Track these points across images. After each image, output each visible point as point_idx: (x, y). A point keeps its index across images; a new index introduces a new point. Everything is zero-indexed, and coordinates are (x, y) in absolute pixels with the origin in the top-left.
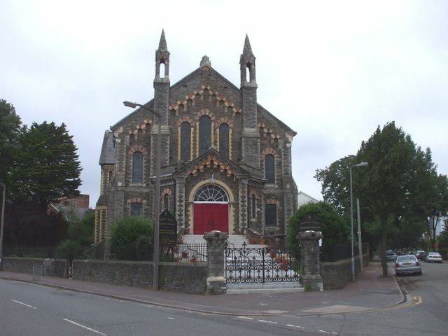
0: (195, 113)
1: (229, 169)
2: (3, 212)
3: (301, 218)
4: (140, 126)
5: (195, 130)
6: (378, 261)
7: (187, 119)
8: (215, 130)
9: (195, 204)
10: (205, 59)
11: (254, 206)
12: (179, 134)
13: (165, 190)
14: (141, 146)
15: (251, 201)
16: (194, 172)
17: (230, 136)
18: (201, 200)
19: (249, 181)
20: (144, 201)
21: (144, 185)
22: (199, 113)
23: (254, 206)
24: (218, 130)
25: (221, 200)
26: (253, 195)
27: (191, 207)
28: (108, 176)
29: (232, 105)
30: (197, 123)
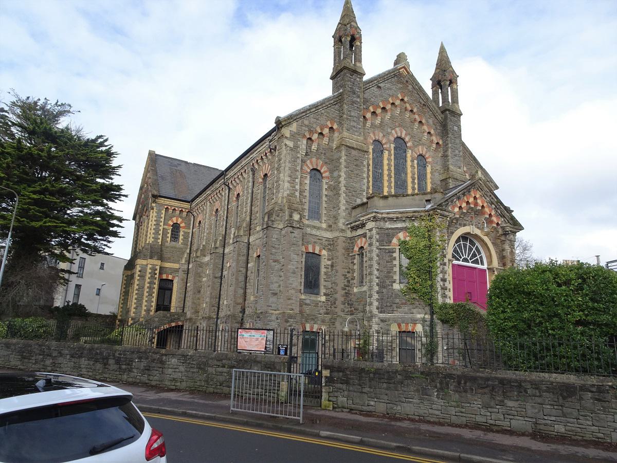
0: (389, 130)
2: (344, 435)
3: (136, 256)
4: (322, 129)
5: (390, 155)
7: (379, 136)
8: (412, 161)
10: (401, 58)
13: (359, 241)
14: (314, 160)
17: (429, 176)
20: (324, 252)
21: (324, 226)
24: (416, 162)
28: (163, 216)
30: (393, 146)
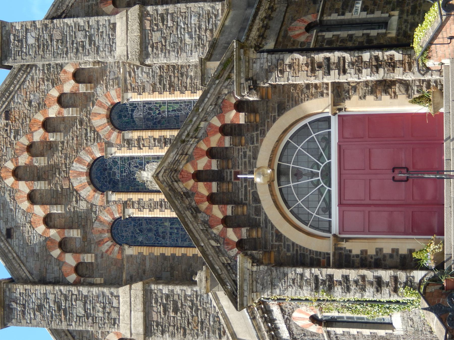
1: (194, 165)
6: (45, 187)
8: (129, 143)
9: (342, 229)
11: (341, 25)
12: (145, 250)
15: (328, 35)
16: (232, 235)
18: (327, 209)
19: (259, 49)
22: (83, 193)
23: (341, 25)
25: (327, 140)
26: (309, 28)
27: (346, 245)
29: (55, 93)
30: (114, 197)
